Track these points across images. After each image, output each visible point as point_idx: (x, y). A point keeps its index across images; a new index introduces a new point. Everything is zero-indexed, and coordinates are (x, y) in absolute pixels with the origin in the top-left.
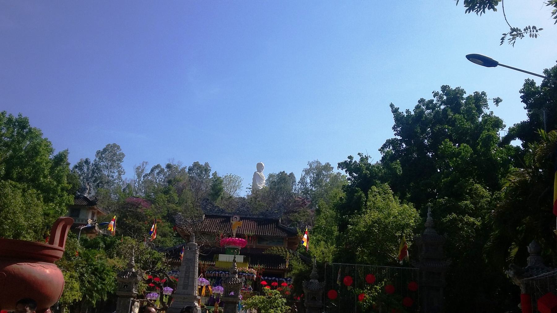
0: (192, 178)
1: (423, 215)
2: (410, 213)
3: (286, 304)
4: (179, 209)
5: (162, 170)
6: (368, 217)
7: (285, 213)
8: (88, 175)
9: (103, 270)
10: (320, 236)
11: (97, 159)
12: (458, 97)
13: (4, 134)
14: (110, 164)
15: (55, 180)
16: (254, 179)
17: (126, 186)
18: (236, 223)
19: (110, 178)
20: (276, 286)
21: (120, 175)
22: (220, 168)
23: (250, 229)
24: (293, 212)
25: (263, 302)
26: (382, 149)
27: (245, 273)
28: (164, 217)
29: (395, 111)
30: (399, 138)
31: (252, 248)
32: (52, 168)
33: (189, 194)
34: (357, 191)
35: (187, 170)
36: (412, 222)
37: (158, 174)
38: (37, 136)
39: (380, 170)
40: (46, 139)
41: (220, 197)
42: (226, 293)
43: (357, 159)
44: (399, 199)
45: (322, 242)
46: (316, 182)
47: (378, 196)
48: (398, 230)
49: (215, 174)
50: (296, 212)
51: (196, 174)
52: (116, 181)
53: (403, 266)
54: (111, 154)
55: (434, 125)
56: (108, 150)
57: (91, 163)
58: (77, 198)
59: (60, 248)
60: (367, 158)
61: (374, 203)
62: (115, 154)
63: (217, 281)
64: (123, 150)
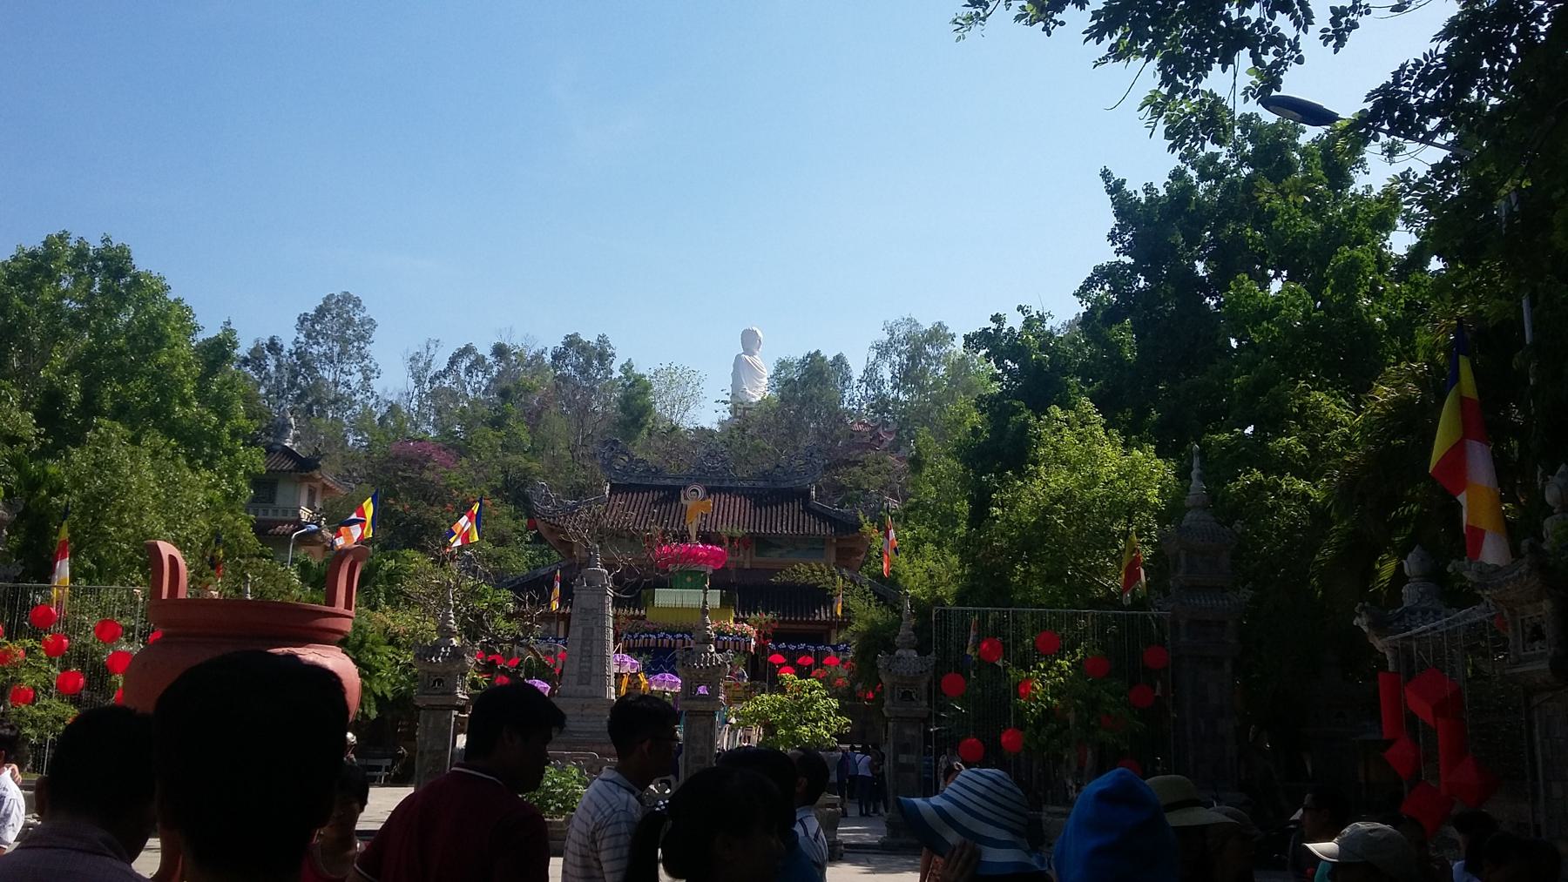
0: (564, 379)
1: (1183, 474)
2: (1152, 472)
3: (839, 712)
4: (535, 466)
5: (480, 360)
6: (1049, 481)
7: (827, 468)
8: (279, 382)
9: (362, 643)
10: (921, 530)
11: (302, 339)
12: (1285, 144)
13: (66, 291)
14: (337, 349)
15: (214, 411)
16: (736, 375)
17: (385, 410)
18: (696, 506)
19: (342, 389)
20: (809, 667)
21: (367, 378)
22: (638, 350)
23: (735, 520)
24: (848, 463)
25: (782, 709)
26: (1082, 292)
27: (727, 634)
28: (496, 492)
29: (1116, 189)
30: (1128, 260)
31: (740, 570)
32: (203, 381)
33: (558, 425)
34: (1017, 411)
35: (548, 358)
36: (1153, 496)
37: (468, 371)
38: (156, 293)
39: (1079, 349)
40: (178, 301)
41: (645, 431)
42: (689, 689)
43: (1015, 322)
44: (1121, 434)
45: (929, 547)
46: (909, 376)
47: (1066, 431)
48: (1116, 518)
49: (627, 368)
50: (855, 463)
51: (575, 368)
52: (359, 397)
53: (1129, 608)
54: (338, 323)
55: (1221, 224)
56: (329, 311)
57: (286, 349)
58: (270, 450)
59: (347, 612)
60: (1042, 319)
61: (1056, 449)
62: (349, 322)
63: (658, 658)
64: (371, 309)
